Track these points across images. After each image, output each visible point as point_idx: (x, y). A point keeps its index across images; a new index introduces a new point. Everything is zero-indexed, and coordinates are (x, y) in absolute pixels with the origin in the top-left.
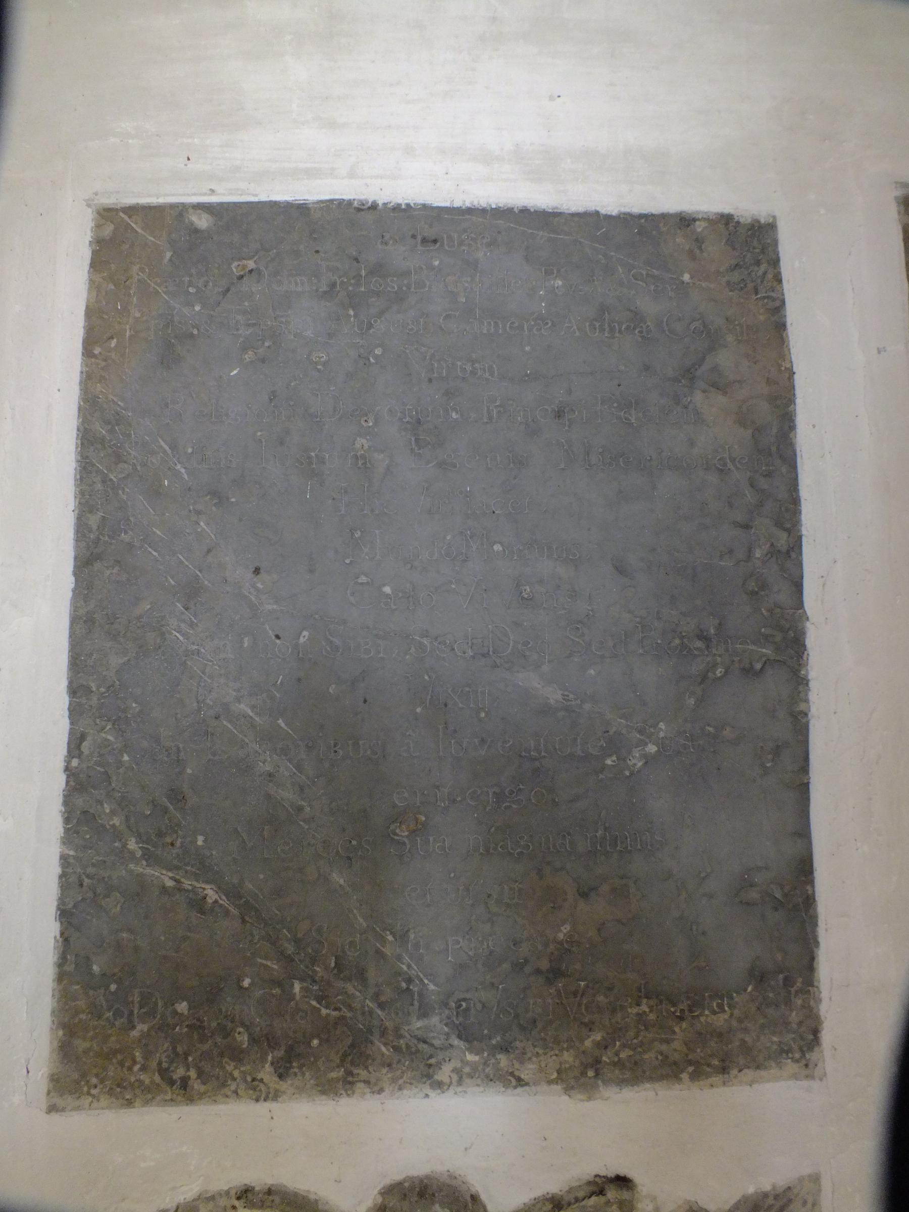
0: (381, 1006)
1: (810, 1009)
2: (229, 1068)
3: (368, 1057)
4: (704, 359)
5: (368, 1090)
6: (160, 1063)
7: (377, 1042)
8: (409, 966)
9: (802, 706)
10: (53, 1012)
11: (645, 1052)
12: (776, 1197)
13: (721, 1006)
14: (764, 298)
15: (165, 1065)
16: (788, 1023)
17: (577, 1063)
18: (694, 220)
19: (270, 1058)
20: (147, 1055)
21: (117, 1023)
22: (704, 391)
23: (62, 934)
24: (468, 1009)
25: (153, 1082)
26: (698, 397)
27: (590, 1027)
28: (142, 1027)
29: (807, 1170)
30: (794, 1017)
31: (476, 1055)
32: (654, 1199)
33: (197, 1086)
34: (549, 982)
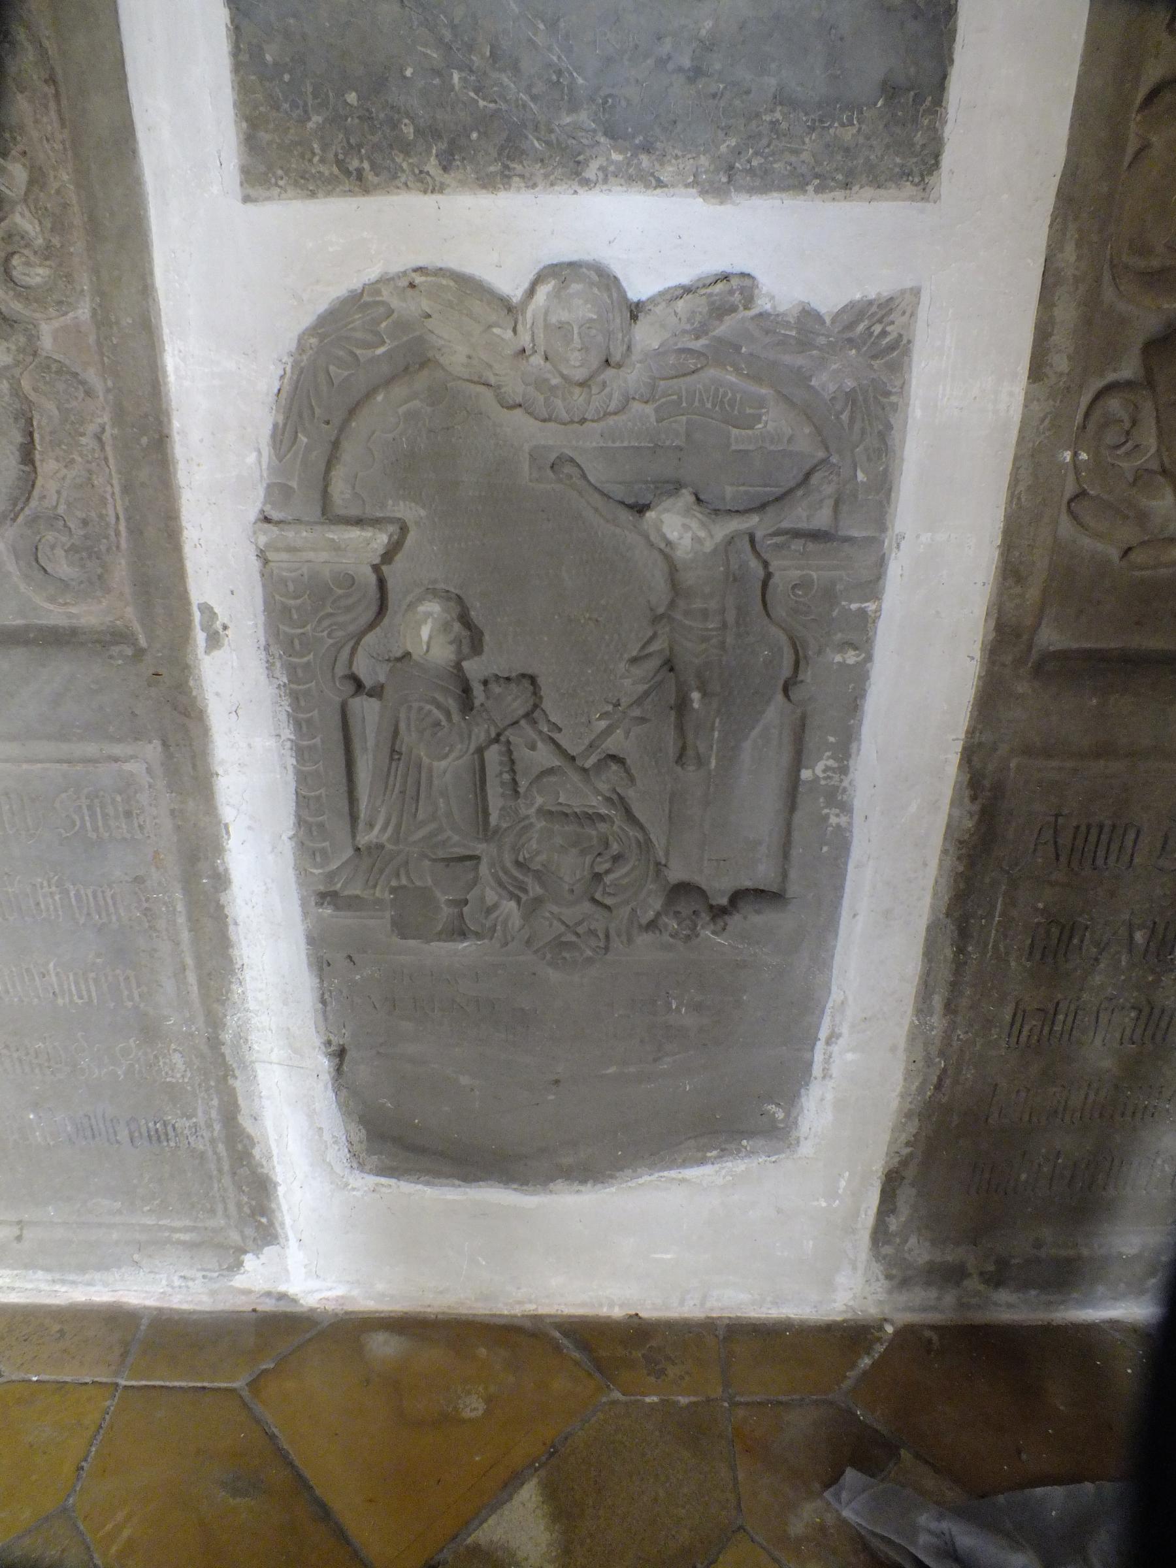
0: (534, 98)
1: (935, 130)
2: (398, 160)
3: (523, 152)
5: (523, 185)
6: (336, 155)
7: (530, 137)
8: (559, 58)
10: (235, 104)
11: (775, 161)
12: (879, 306)
15: (341, 157)
16: (913, 145)
19: (434, 151)
20: (325, 147)
21: (294, 115)
23: (232, 21)
24: (613, 106)
25: (331, 174)
27: (727, 131)
28: (316, 119)
29: (909, 284)
30: (919, 138)
31: (620, 153)
32: (773, 298)
33: (370, 177)
34: (692, 80)
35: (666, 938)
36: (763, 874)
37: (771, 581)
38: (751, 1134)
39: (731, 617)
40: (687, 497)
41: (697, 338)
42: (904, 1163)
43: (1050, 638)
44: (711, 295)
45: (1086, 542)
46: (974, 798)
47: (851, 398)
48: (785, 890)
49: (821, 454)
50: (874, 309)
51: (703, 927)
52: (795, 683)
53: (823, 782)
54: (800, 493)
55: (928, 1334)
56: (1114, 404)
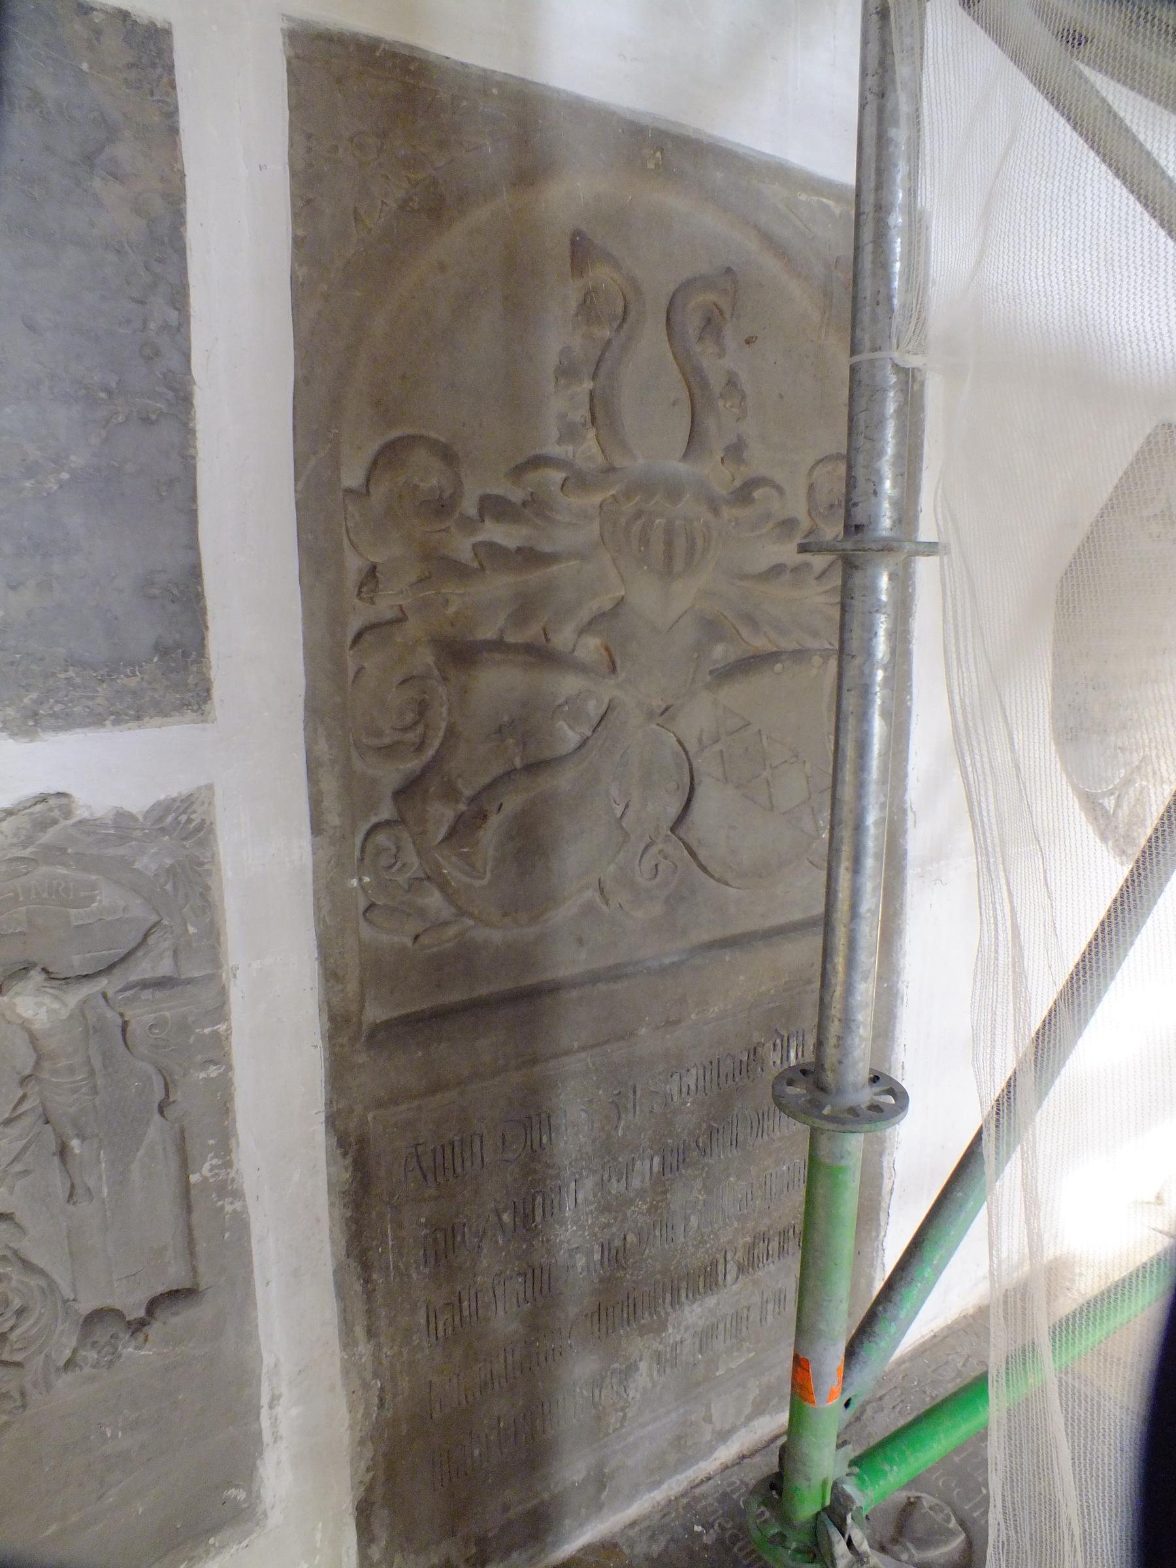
1: (203, 673)
4: (103, 148)
9: (191, 452)
12: (182, 801)
13: (133, 672)
14: (159, 101)
17: (18, 716)
18: (92, 9)
22: (103, 179)
26: (97, 183)
27: (27, 688)
29: (203, 782)
30: (191, 680)
35: (87, 1370)
36: (175, 1275)
37: (129, 1029)
38: (214, 1530)
39: (97, 1063)
40: (36, 977)
41: (25, 847)
42: (370, 1489)
43: (375, 1013)
44: (32, 814)
45: (385, 938)
46: (345, 1154)
47: (171, 871)
48: (198, 1285)
49: (154, 918)
50: (178, 804)
51: (124, 1347)
52: (169, 1104)
53: (212, 1180)
54: (140, 953)
56: (381, 838)
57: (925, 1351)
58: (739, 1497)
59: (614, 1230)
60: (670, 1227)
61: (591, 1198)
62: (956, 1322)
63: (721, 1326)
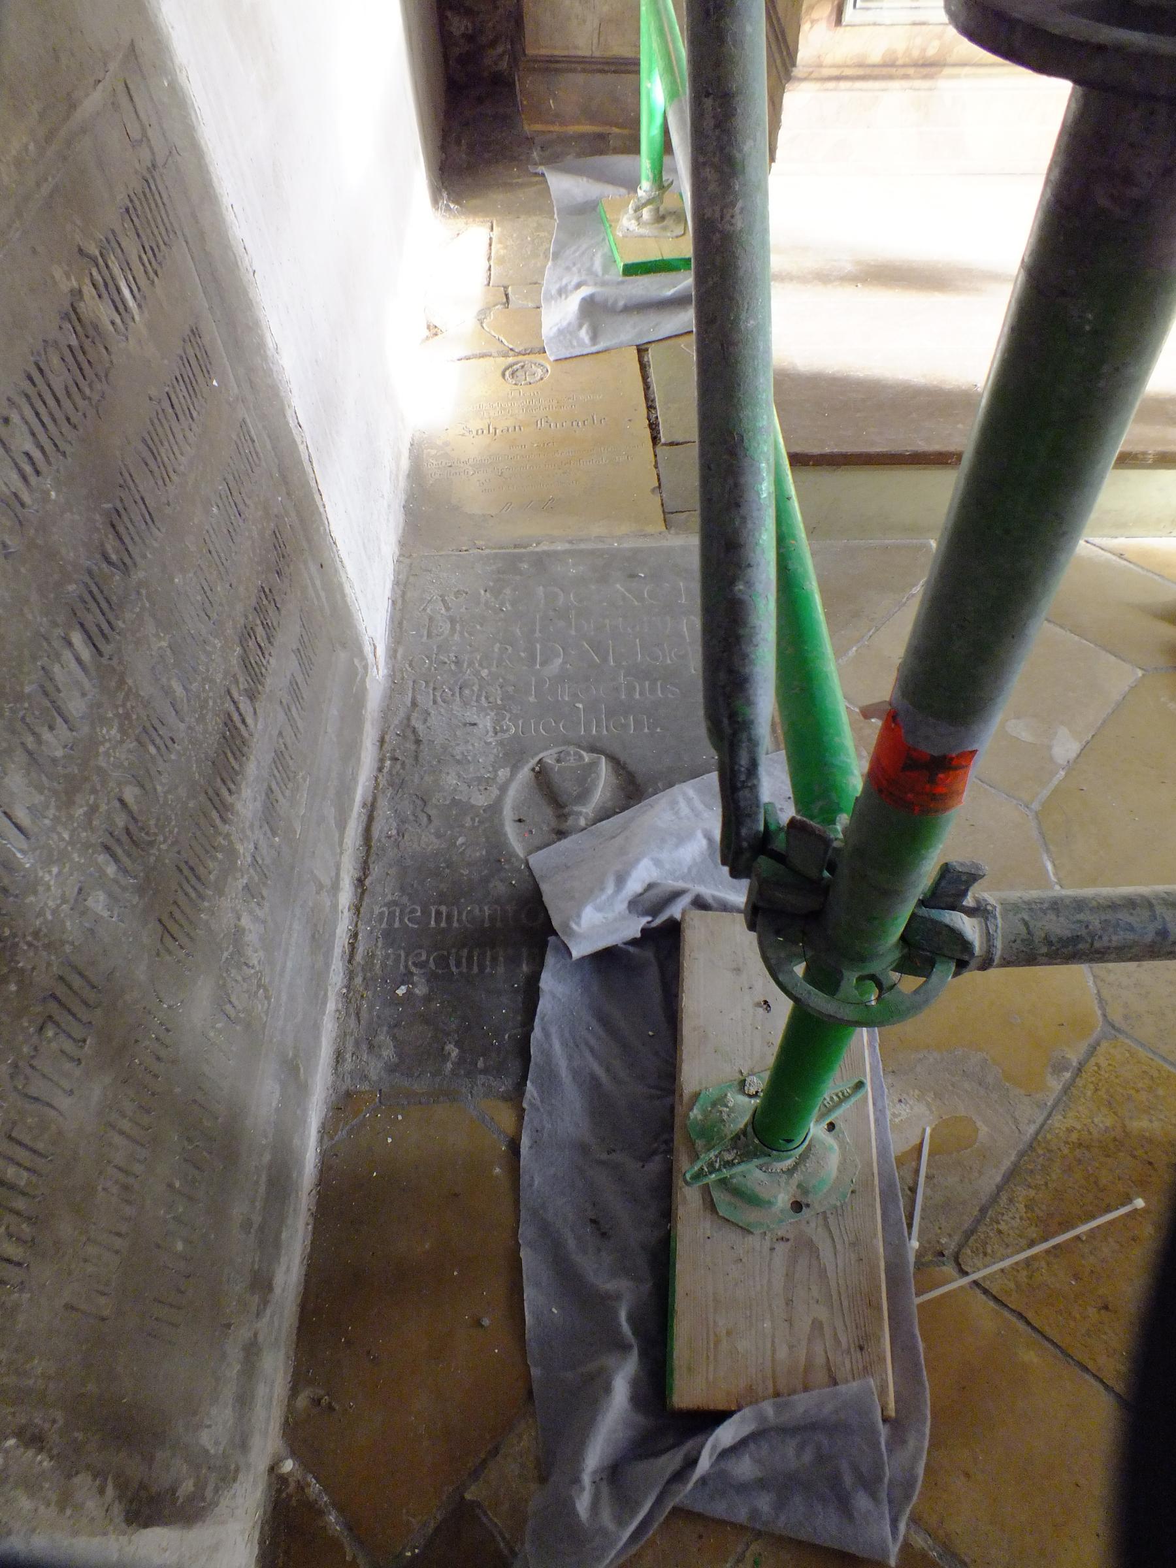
55: (302, 1402)
57: (400, 623)
58: (401, 920)
59: (103, 808)
60: (158, 726)
61: (38, 799)
62: (397, 573)
63: (274, 786)
